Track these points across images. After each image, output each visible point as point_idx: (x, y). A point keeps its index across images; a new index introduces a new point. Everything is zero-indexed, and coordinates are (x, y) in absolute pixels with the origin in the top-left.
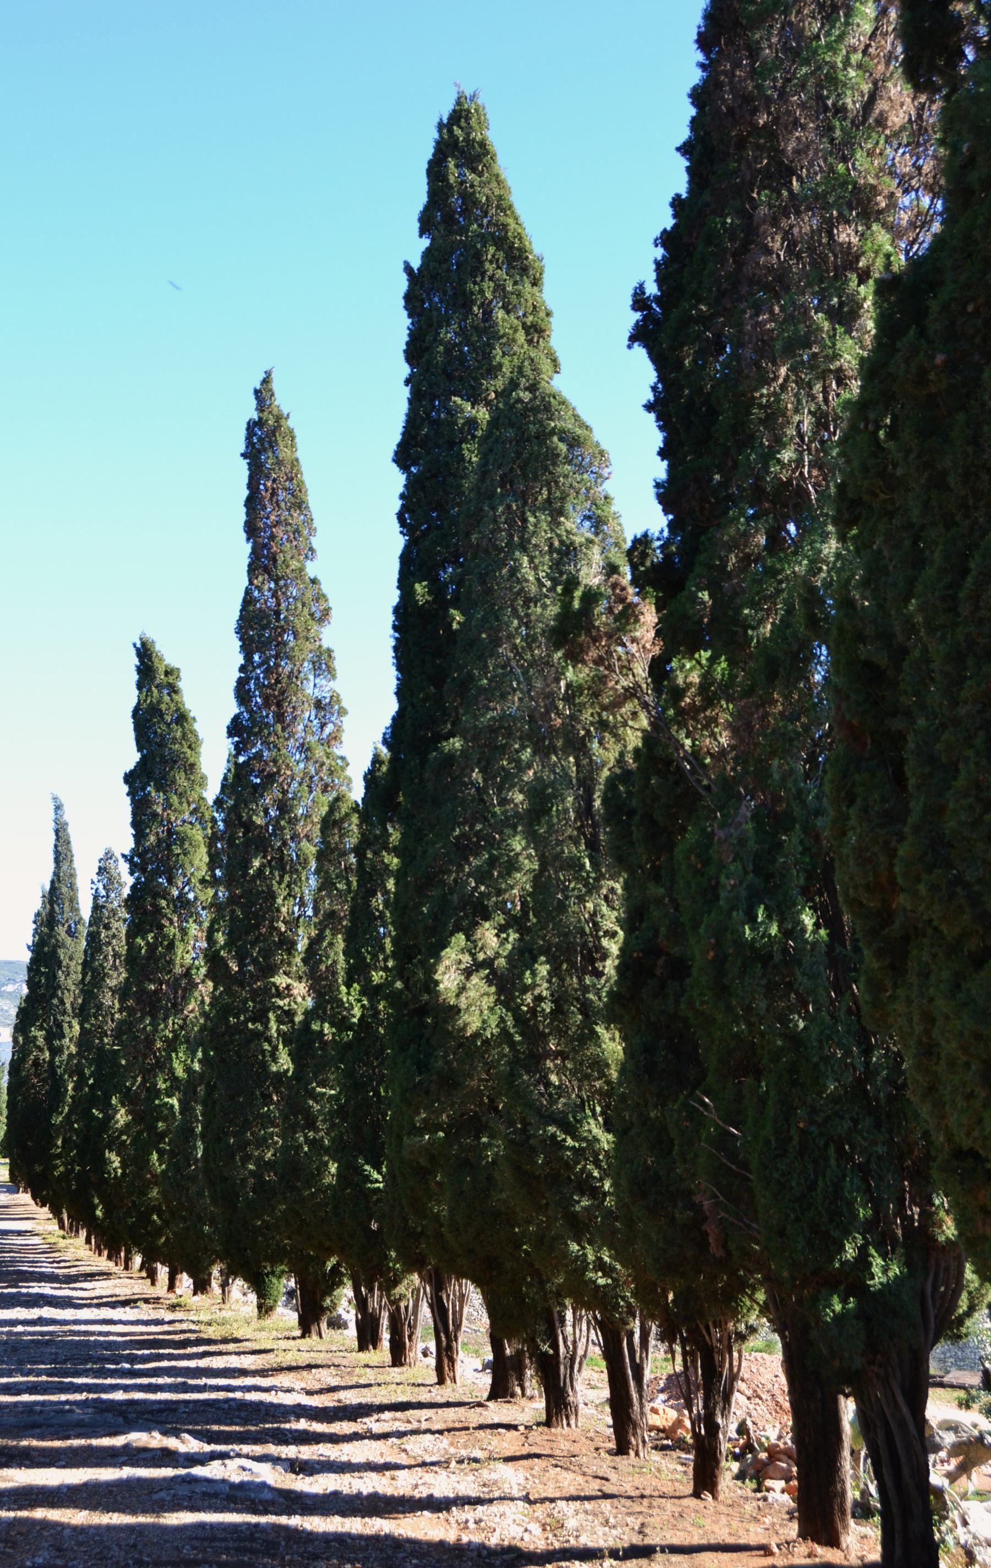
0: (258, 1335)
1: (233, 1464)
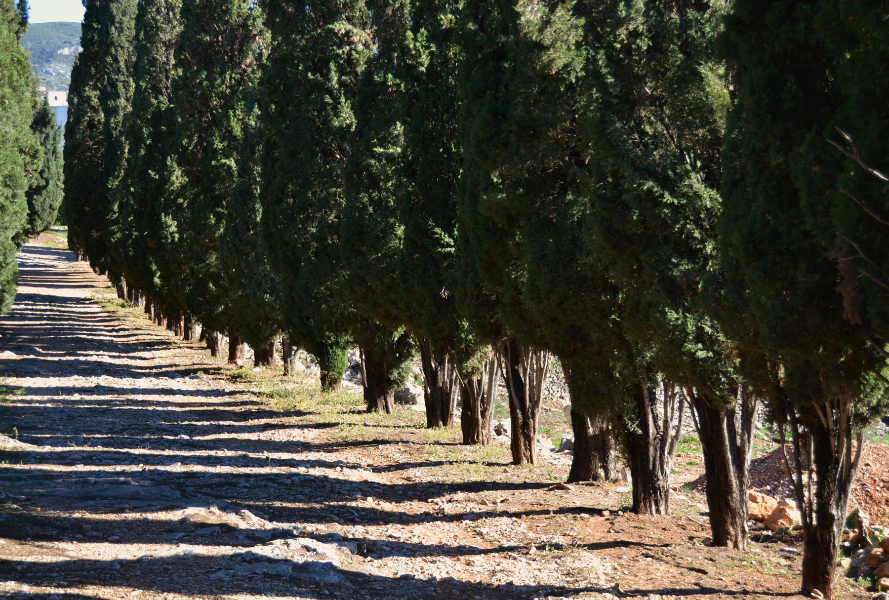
0: (321, 408)
1: (296, 544)
